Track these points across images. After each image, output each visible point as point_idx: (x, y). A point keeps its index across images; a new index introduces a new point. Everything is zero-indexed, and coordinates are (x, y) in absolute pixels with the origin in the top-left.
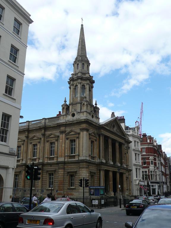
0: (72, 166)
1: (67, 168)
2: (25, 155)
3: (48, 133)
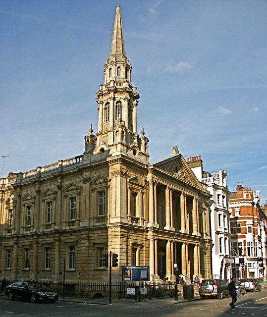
0: (100, 235)
1: (93, 238)
2: (36, 221)
3: (66, 183)
